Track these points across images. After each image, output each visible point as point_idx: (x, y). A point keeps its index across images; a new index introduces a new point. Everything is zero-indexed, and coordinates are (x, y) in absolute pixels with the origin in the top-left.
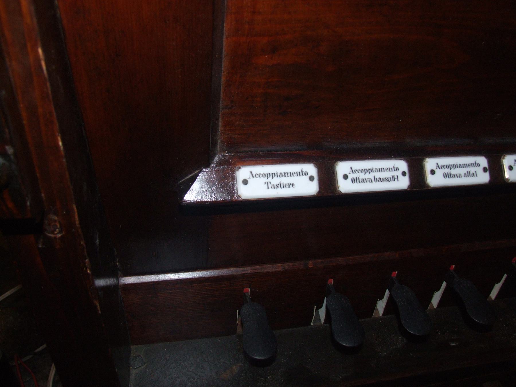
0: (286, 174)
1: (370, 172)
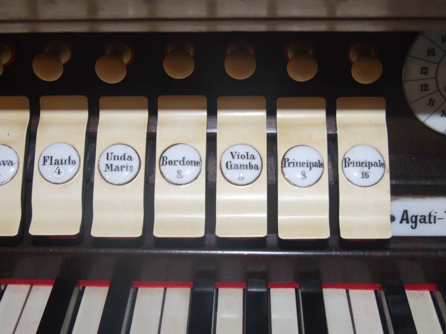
0: (242, 166)
1: (370, 165)
